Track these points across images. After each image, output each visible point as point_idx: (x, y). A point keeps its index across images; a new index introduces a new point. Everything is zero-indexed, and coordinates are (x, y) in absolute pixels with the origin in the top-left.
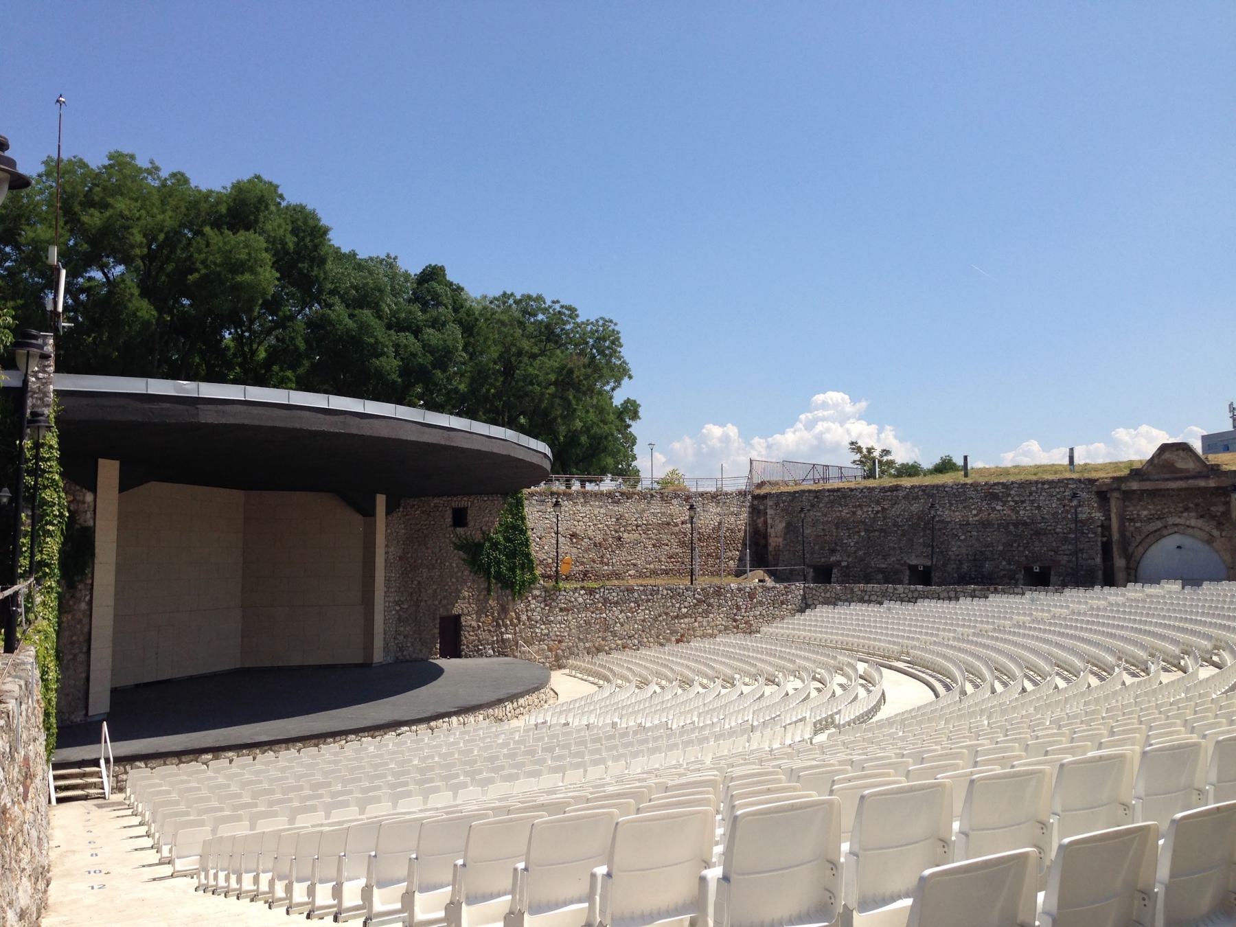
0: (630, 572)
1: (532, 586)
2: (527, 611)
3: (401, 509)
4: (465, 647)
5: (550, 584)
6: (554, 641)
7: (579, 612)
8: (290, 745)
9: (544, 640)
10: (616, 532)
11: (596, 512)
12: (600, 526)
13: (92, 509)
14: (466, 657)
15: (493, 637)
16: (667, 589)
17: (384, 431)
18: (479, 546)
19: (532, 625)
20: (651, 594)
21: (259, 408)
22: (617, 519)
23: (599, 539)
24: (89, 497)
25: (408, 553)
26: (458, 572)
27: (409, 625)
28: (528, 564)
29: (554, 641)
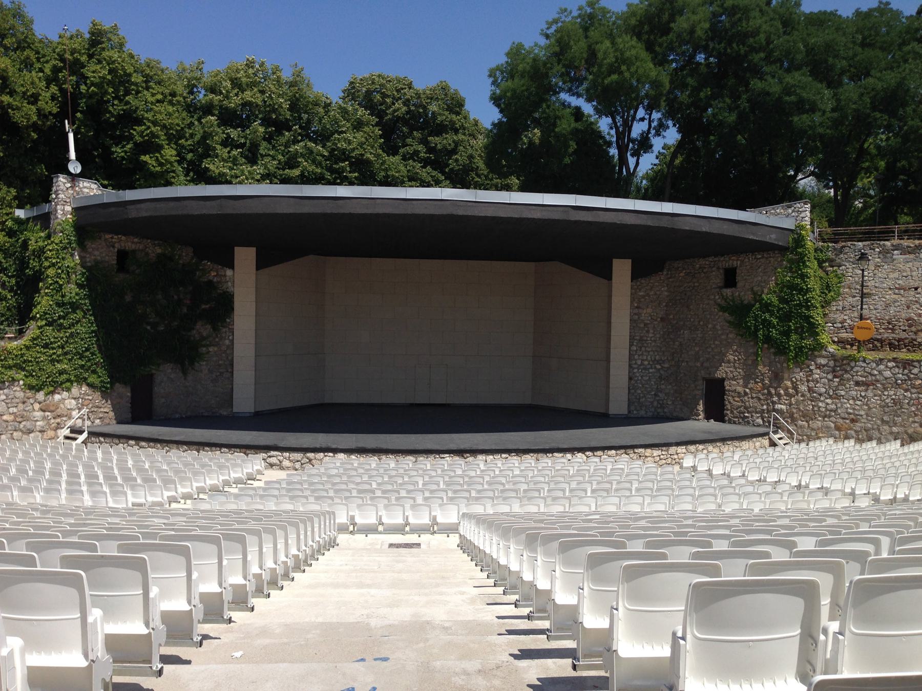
1: (816, 353)
2: (808, 381)
3: (665, 273)
7: (885, 389)
9: (830, 416)
14: (730, 423)
15: (762, 405)
18: (749, 307)
19: (814, 397)
24: (229, 272)
27: (670, 384)
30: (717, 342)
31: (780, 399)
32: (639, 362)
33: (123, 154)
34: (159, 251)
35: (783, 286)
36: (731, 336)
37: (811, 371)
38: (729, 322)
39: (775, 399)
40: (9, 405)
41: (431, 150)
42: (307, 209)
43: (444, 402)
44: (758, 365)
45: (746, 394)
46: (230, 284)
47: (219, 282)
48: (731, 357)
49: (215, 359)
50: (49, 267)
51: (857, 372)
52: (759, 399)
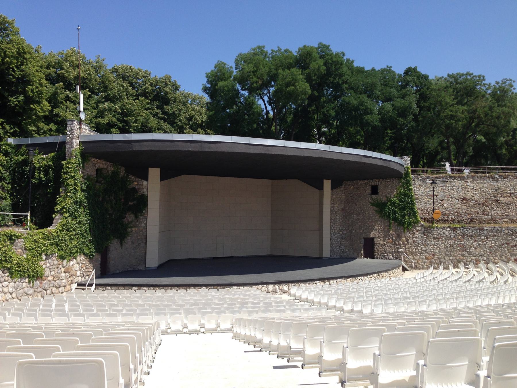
0: (504, 220)
1: (416, 225)
2: (413, 238)
3: (343, 187)
4: (376, 254)
5: (426, 224)
6: (429, 254)
7: (446, 240)
8: (172, 288)
9: (423, 253)
10: (495, 197)
11: (481, 186)
12: (483, 194)
13: (146, 187)
14: (377, 258)
15: (392, 250)
16: (508, 230)
17: (225, 149)
18: (385, 204)
19: (416, 245)
20: (497, 232)
21: (158, 142)
22: (496, 190)
23: (482, 200)
24: (145, 183)
25: (346, 207)
26: (372, 217)
27: (347, 241)
28: (413, 213)
29: (429, 254)
30: (370, 221)
31: (400, 246)
32: (334, 231)
33: (17, 102)
34: (112, 169)
35: (401, 194)
36: (377, 217)
37: (414, 233)
38: (376, 211)
39: (398, 246)
40: (51, 270)
41: (164, 113)
42: (252, 150)
43: (230, 256)
44: (390, 231)
45: (384, 244)
46: (145, 190)
47: (139, 189)
48: (377, 228)
49: (135, 235)
50: (69, 179)
51: (434, 233)
52: (391, 247)
